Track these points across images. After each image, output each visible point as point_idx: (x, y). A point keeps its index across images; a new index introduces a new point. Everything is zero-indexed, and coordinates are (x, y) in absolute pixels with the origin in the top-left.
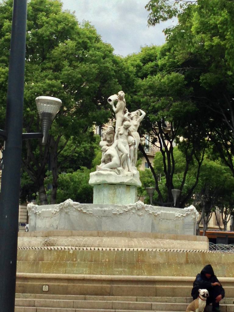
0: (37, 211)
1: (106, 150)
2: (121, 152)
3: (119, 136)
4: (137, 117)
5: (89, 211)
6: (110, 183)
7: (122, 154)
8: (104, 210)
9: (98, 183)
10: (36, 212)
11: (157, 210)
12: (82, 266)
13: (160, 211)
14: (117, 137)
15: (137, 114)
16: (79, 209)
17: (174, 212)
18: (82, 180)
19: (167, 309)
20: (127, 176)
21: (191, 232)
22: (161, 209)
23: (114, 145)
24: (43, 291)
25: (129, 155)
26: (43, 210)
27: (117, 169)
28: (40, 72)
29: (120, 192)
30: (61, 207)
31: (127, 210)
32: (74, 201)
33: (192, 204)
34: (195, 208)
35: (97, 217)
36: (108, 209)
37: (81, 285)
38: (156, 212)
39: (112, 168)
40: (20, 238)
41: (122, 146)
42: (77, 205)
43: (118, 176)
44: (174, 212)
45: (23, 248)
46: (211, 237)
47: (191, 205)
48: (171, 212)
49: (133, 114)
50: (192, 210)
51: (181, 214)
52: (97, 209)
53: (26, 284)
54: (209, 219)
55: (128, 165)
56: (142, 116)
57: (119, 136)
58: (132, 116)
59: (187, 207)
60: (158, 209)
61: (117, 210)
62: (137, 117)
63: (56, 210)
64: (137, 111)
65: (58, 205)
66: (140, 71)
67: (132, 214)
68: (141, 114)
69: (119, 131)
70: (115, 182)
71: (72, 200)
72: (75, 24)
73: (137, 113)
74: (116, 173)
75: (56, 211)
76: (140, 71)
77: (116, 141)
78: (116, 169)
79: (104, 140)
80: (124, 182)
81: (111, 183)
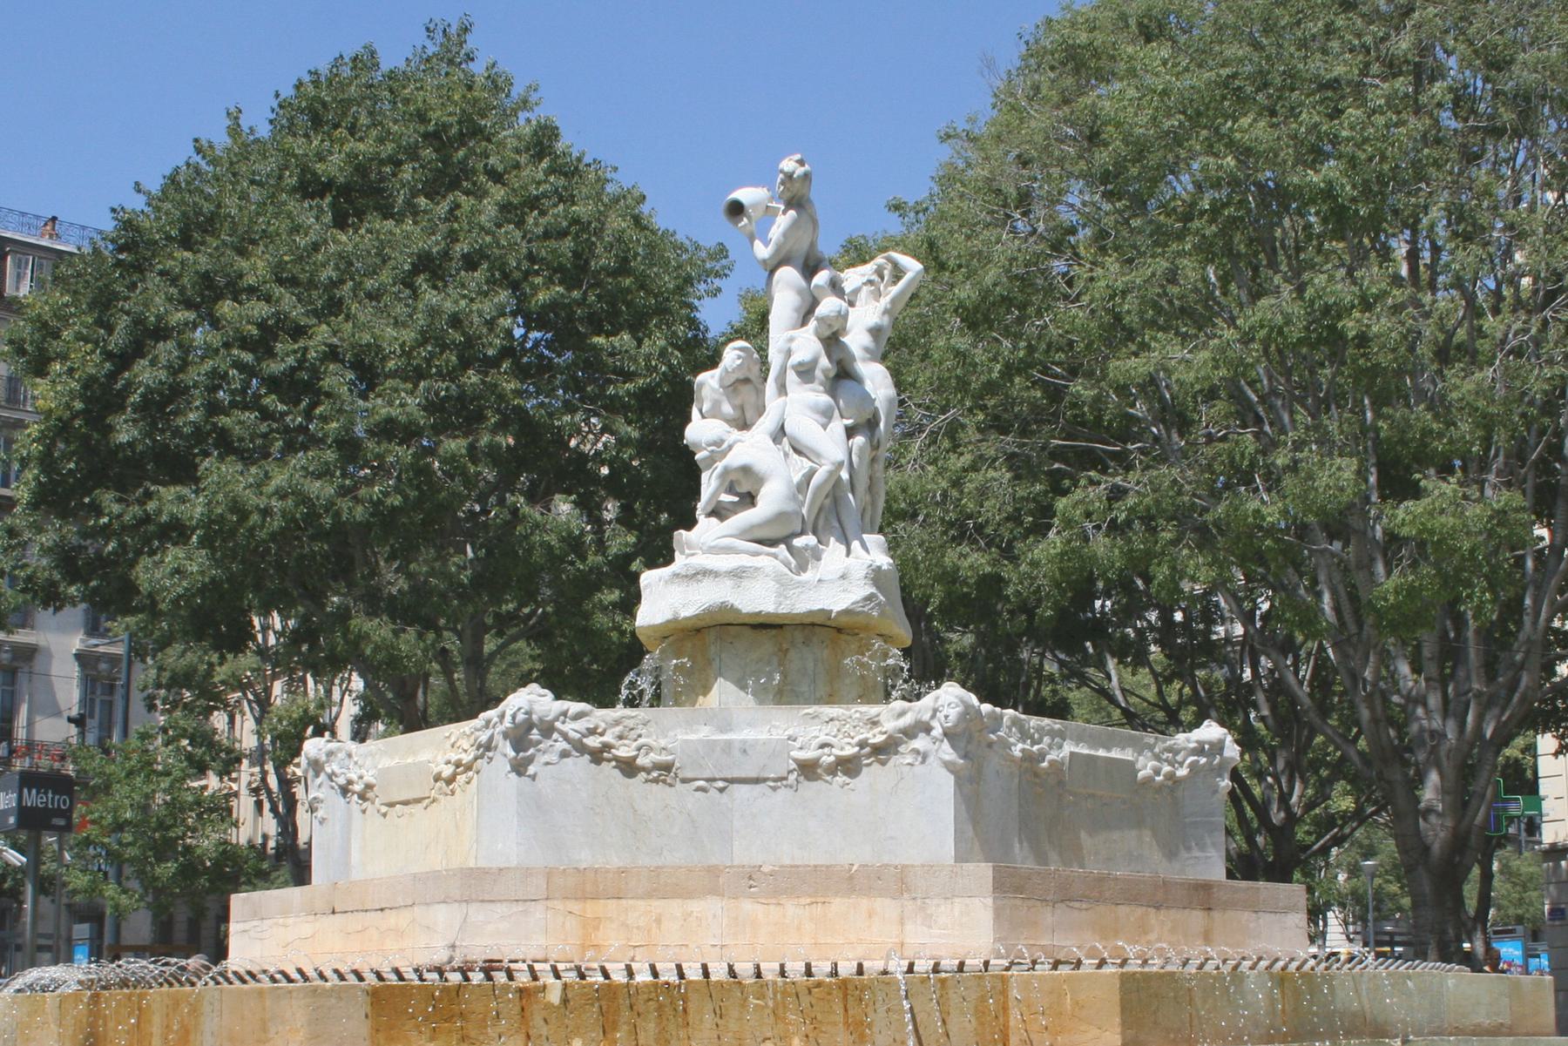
0: (354, 777)
1: (725, 446)
2: (805, 460)
4: (878, 295)
5: (650, 749)
6: (752, 621)
7: (807, 464)
8: (744, 742)
9: (686, 619)
10: (350, 782)
13: (1060, 747)
14: (782, 389)
15: (875, 278)
16: (593, 742)
17: (1127, 755)
20: (843, 577)
22: (1062, 735)
23: (766, 424)
26: (386, 762)
27: (790, 549)
28: (531, 656)
29: (810, 665)
31: (880, 739)
32: (558, 697)
33: (1208, 717)
34: (1229, 738)
35: (702, 783)
36: (764, 736)
40: (240, 926)
41: (804, 426)
42: (579, 716)
43: (796, 577)
44: (1127, 755)
45: (296, 976)
47: (1206, 723)
48: (1115, 754)
50: (1218, 747)
51: (1166, 768)
52: (701, 735)
53: (860, 457)
56: (901, 284)
59: (1190, 731)
60: (1053, 734)
61: (823, 738)
63: (454, 757)
64: (880, 260)
65: (466, 726)
67: (909, 760)
68: (898, 271)
69: (789, 353)
70: (783, 610)
71: (546, 691)
74: (787, 565)
75: (458, 764)
77: (773, 403)
78: (783, 546)
80: (826, 613)
81: (761, 620)
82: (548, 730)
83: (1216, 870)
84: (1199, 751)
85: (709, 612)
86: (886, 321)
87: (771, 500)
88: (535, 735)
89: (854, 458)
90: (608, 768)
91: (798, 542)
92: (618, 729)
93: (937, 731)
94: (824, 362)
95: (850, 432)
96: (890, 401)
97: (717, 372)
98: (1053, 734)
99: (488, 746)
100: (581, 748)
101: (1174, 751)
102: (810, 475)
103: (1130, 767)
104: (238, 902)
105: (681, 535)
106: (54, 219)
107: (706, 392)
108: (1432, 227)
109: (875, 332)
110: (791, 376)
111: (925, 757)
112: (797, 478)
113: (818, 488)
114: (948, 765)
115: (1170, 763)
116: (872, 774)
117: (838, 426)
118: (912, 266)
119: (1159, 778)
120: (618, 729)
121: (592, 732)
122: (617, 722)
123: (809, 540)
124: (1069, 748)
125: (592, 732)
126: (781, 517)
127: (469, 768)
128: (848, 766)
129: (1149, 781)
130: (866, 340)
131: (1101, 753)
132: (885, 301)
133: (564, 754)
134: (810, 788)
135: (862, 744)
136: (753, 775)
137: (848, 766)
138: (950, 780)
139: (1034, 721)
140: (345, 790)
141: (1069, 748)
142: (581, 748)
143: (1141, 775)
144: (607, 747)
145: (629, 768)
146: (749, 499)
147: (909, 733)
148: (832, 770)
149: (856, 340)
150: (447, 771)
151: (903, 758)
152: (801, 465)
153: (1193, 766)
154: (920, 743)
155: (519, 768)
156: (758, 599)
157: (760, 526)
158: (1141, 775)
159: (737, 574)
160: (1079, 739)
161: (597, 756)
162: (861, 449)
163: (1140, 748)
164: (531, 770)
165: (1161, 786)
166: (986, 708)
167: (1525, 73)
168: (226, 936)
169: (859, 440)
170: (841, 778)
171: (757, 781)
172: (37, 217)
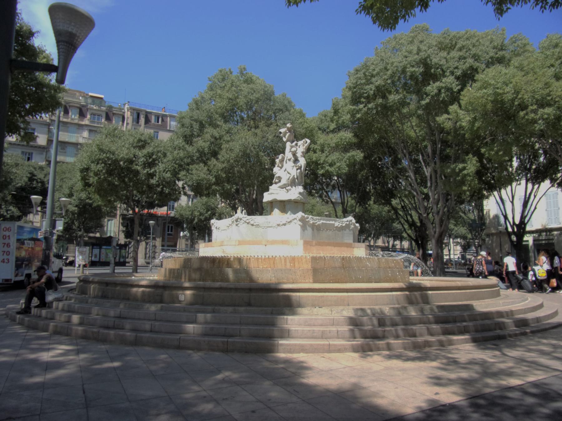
14: (286, 163)
16: (248, 221)
17: (333, 222)
18: (174, 170)
19: (307, 324)
21: (349, 239)
22: (321, 219)
25: (296, 177)
37: (218, 293)
38: (316, 223)
39: (282, 187)
41: (289, 170)
44: (333, 222)
46: (536, 253)
48: (331, 222)
49: (300, 143)
50: (351, 221)
51: (341, 224)
54: (522, 378)
57: (288, 161)
58: (299, 145)
64: (304, 140)
68: (306, 142)
73: (304, 142)
80: (291, 200)
82: (241, 219)
83: (351, 241)
84: (347, 221)
85: (273, 200)
86: (304, 150)
87: (283, 181)
88: (239, 220)
91: (287, 188)
93: (298, 220)
94: (293, 158)
95: (297, 169)
98: (318, 219)
100: (245, 222)
101: (343, 221)
103: (334, 224)
104: (546, 278)
105: (270, 187)
107: (277, 163)
109: (303, 152)
110: (288, 161)
114: (300, 225)
116: (288, 226)
118: (309, 141)
123: (290, 187)
124: (322, 221)
126: (285, 184)
130: (301, 154)
131: (328, 222)
132: (304, 147)
134: (279, 227)
139: (315, 218)
140: (216, 228)
141: (322, 221)
142: (245, 222)
146: (280, 181)
147: (294, 220)
148: (282, 225)
150: (228, 225)
151: (293, 223)
152: (289, 175)
153: (346, 224)
154: (295, 221)
156: (280, 198)
157: (282, 185)
160: (324, 220)
161: (248, 223)
163: (336, 221)
164: (239, 225)
165: (340, 227)
167: (518, 49)
168: (528, 308)
170: (283, 226)
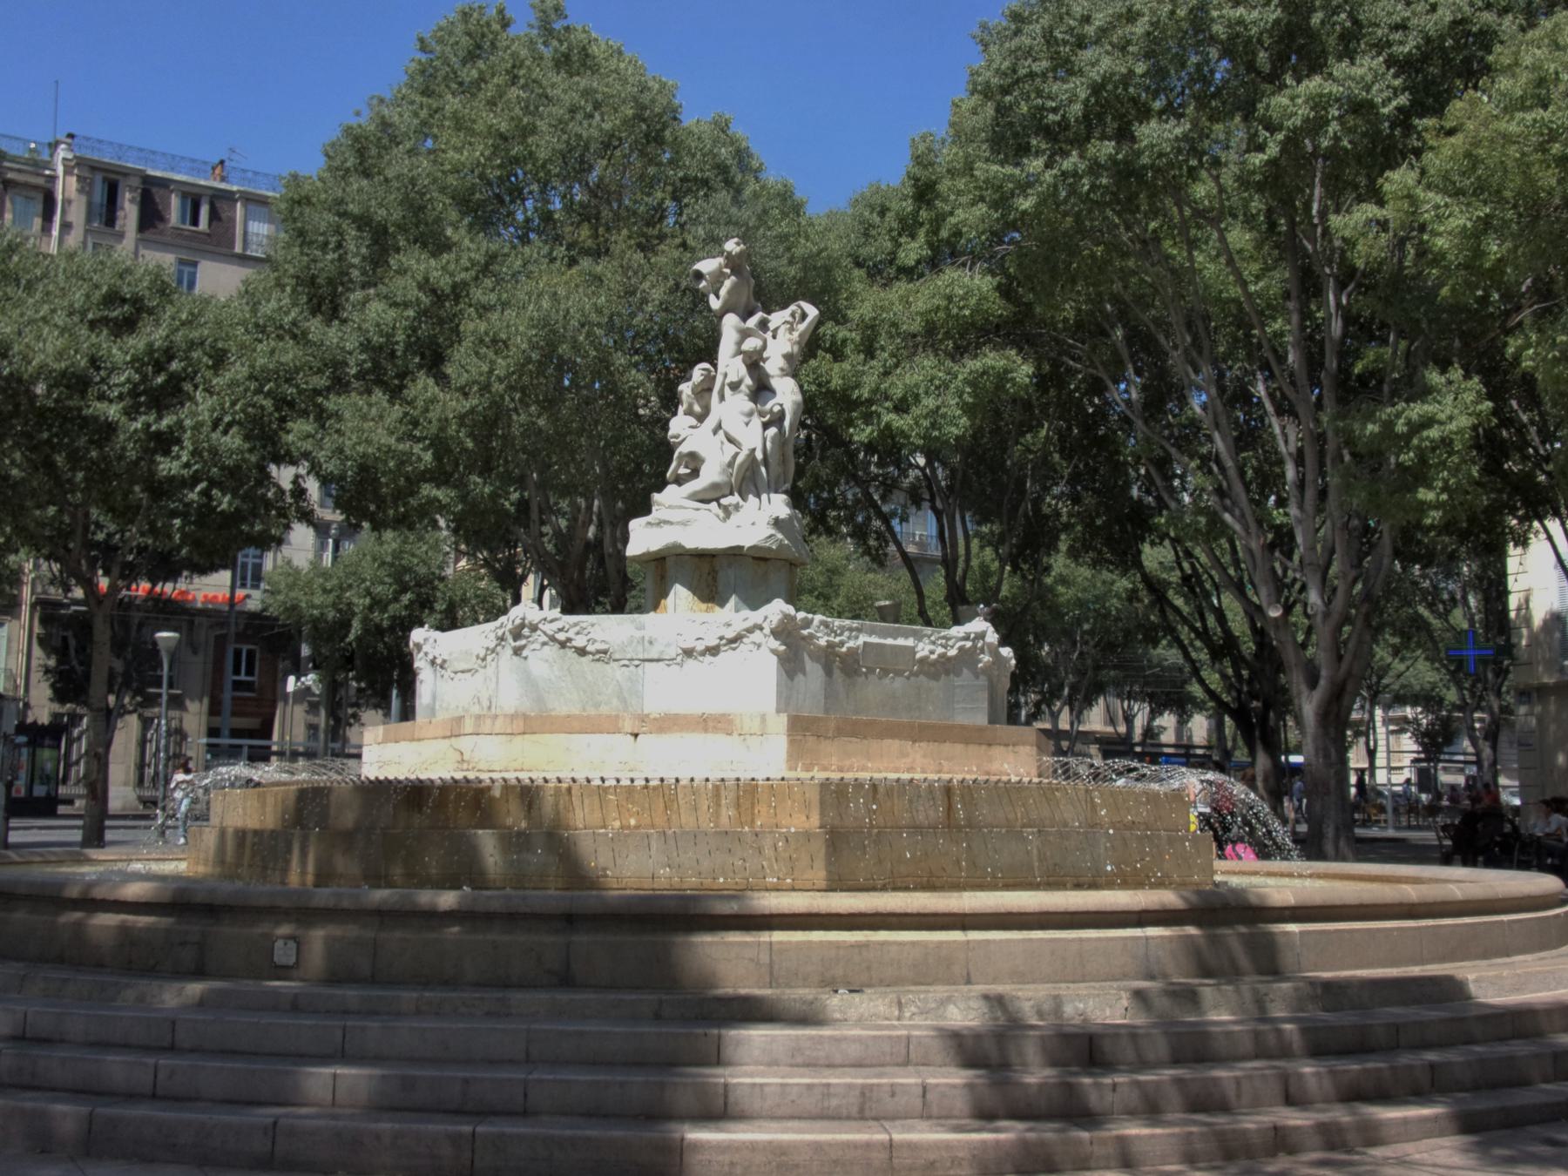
3: (727, 390)
4: (791, 330)
5: (595, 641)
11: (847, 634)
12: (1200, 727)
14: (722, 398)
16: (561, 636)
17: (910, 642)
22: (859, 630)
23: (710, 422)
24: (277, 967)
30: (500, 633)
38: (842, 643)
39: (703, 498)
41: (734, 426)
44: (910, 642)
48: (901, 642)
49: (778, 318)
51: (940, 650)
55: (181, 247)
57: (727, 390)
62: (791, 330)
64: (793, 307)
66: (1248, 647)
68: (804, 316)
72: (673, 113)
73: (793, 315)
76: (1248, 647)
78: (714, 504)
79: (686, 413)
83: (981, 719)
86: (796, 348)
87: (711, 474)
88: (526, 631)
89: (769, 445)
90: (570, 653)
91: (724, 501)
92: (577, 629)
93: (767, 631)
94: (748, 381)
95: (766, 426)
96: (795, 403)
97: (690, 384)
98: (851, 629)
99: (502, 639)
100: (553, 639)
102: (737, 454)
105: (656, 497)
106: (222, 162)
107: (684, 397)
108: (1514, 106)
111: (759, 646)
112: (727, 459)
113: (741, 465)
114: (774, 652)
115: (945, 646)
116: (726, 656)
117: (757, 422)
119: (934, 657)
120: (577, 629)
121: (561, 630)
122: (576, 625)
125: (561, 630)
126: (715, 486)
127: (493, 651)
128: (713, 651)
129: (923, 660)
130: (782, 363)
131: (889, 641)
132: (796, 335)
133: (544, 644)
134: (690, 663)
135: (721, 638)
136: (655, 656)
137: (713, 651)
138: (775, 658)
139: (837, 622)
140: (433, 662)
143: (918, 656)
144: (569, 640)
145: (582, 652)
146: (695, 473)
147: (750, 631)
148: (703, 654)
149: (774, 365)
151: (744, 647)
153: (961, 649)
154: (757, 636)
155: (517, 651)
157: (705, 490)
158: (918, 656)
159: (684, 523)
160: (871, 632)
161: (563, 645)
162: (773, 439)
163: (919, 637)
164: (525, 653)
165: (936, 661)
166: (801, 615)
169: (773, 431)
170: (708, 658)
171: (658, 660)
172: (205, 163)
